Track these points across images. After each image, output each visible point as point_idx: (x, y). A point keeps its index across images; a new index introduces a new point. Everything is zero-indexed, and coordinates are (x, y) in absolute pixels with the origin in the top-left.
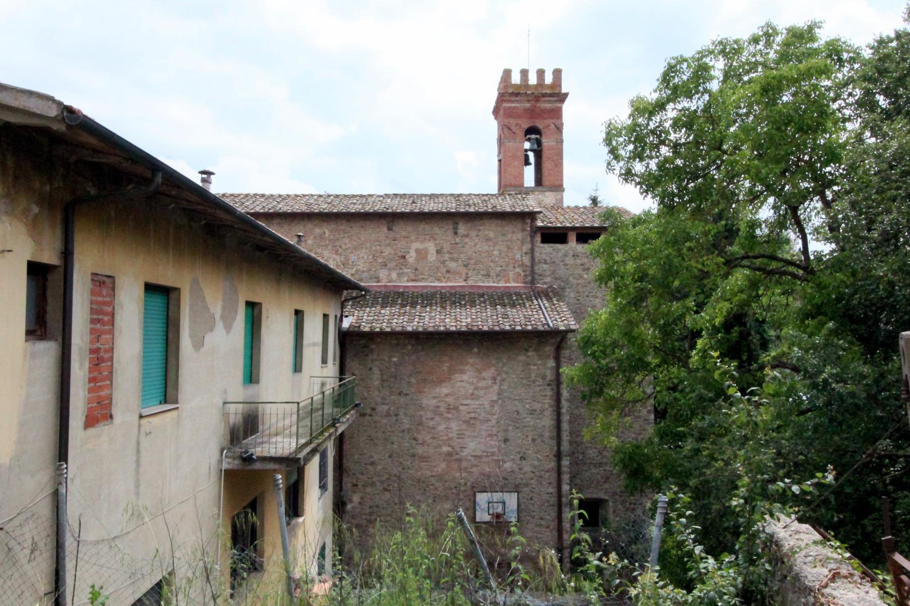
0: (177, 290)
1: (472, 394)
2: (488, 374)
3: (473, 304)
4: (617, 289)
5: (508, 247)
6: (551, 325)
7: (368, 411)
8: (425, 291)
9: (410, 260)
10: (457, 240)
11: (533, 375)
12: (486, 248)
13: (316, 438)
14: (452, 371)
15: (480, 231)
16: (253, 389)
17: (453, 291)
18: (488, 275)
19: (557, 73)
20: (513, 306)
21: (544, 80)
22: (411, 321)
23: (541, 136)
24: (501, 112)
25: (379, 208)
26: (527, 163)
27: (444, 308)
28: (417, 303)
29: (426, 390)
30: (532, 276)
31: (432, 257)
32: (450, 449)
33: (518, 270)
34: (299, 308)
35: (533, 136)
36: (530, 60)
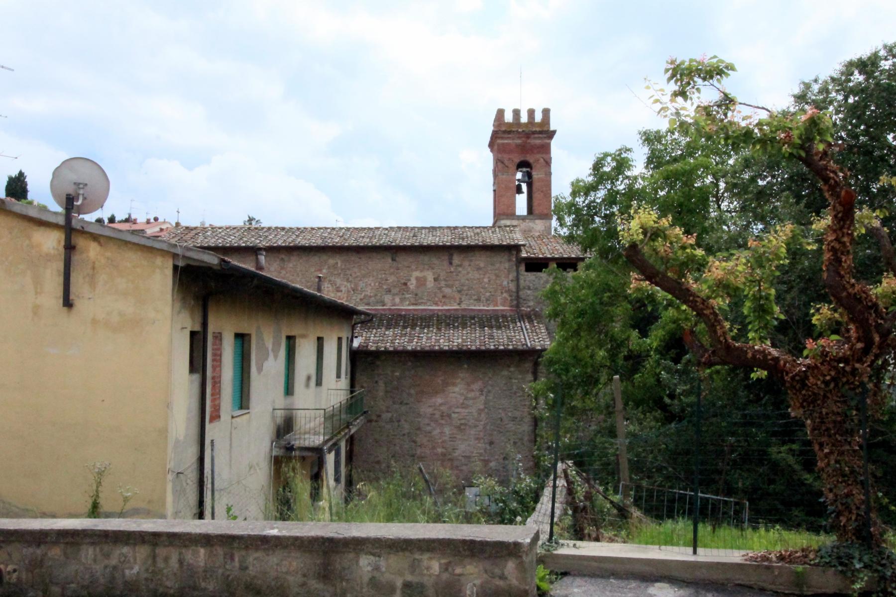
0: (249, 335)
1: (463, 404)
2: (477, 386)
3: (464, 326)
4: (563, 324)
5: (497, 276)
6: (529, 345)
7: (374, 418)
8: (424, 313)
9: (412, 287)
10: (452, 269)
11: (515, 387)
12: (477, 276)
13: (336, 435)
14: (446, 384)
15: (471, 261)
16: (289, 399)
17: (448, 314)
18: (478, 300)
19: (546, 112)
20: (499, 328)
21: (534, 119)
22: (410, 341)
23: (531, 168)
24: (496, 147)
25: (384, 241)
26: (519, 190)
27: (439, 329)
28: (416, 325)
29: (424, 400)
30: (517, 299)
31: (430, 283)
32: (444, 450)
33: (505, 295)
34: (321, 336)
35: (524, 169)
36: (523, 99)
